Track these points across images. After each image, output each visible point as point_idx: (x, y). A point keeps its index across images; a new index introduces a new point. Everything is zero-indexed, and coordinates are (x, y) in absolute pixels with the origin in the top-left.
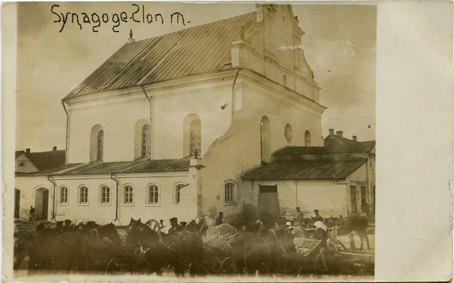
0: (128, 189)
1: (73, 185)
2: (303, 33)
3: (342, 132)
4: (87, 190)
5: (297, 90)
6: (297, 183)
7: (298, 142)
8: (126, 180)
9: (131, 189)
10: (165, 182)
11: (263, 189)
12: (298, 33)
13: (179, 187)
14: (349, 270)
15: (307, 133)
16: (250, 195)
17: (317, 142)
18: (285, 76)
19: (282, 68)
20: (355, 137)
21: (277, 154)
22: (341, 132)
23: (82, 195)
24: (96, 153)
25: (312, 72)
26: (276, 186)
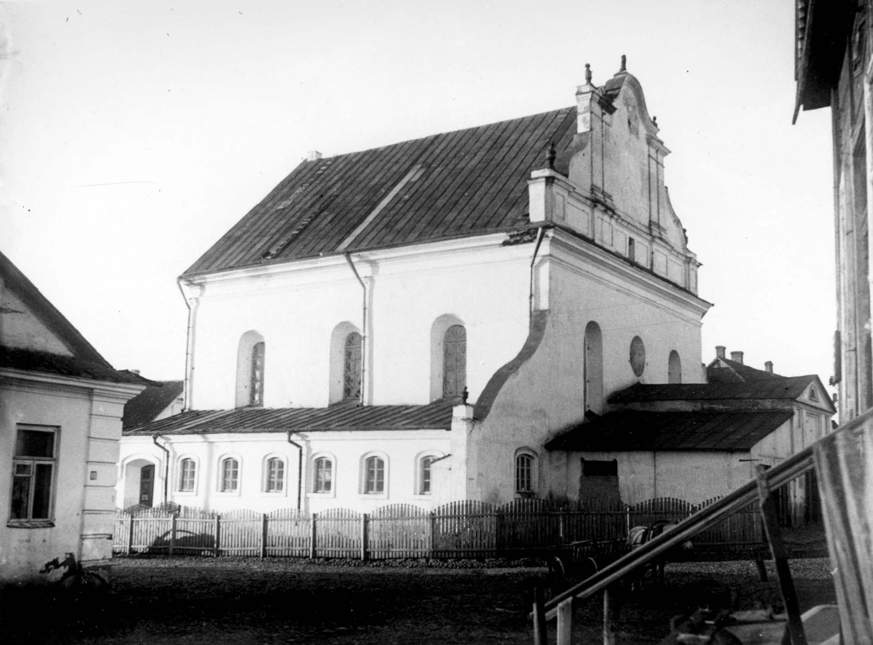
0: (322, 464)
1: (186, 445)
2: (666, 152)
3: (742, 354)
4: (236, 464)
5: (606, 185)
6: (657, 458)
7: (657, 374)
8: (321, 443)
10: (400, 448)
11: (590, 470)
12: (657, 151)
13: (427, 462)
16: (564, 479)
17: (693, 376)
18: (631, 241)
19: (625, 224)
20: (769, 364)
21: (618, 397)
22: (741, 354)
25: (684, 231)
26: (614, 464)
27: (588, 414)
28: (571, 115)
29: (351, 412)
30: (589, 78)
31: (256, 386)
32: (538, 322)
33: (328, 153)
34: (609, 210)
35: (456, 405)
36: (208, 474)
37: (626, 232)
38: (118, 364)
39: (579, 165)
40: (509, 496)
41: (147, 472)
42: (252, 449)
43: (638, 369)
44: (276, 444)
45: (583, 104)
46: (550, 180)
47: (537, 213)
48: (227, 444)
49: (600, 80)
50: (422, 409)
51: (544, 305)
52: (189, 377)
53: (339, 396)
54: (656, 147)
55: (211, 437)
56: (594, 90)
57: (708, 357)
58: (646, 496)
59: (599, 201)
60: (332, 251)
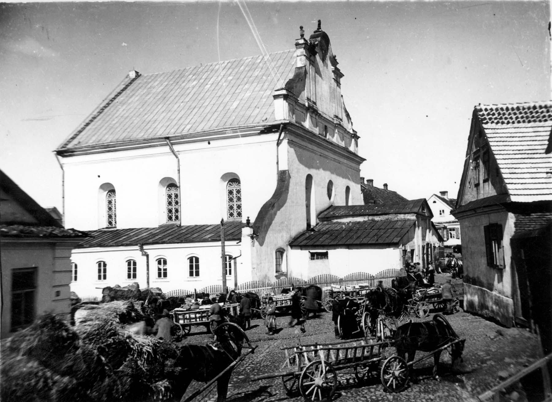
8: (155, 251)
9: (165, 262)
10: (209, 254)
14: (69, 372)
20: (386, 185)
22: (372, 181)
23: (191, 267)
24: (436, 201)
35: (243, 227)
37: (323, 122)
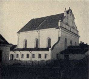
0: (34, 55)
1: (18, 52)
7: (73, 44)
8: (34, 52)
10: (43, 53)
15: (76, 42)
16: (62, 57)
17: (77, 45)
21: (68, 47)
27: (65, 49)
28: (64, 14)
29: (37, 49)
30: (66, 9)
31: (26, 46)
32: (59, 38)
33: (35, 18)
34: (68, 25)
36: (20, 56)
38: (9, 43)
39: (64, 20)
40: (56, 58)
41: (13, 55)
42: (25, 53)
43: (71, 44)
44: (28, 52)
45: (65, 13)
46: (61, 22)
47: (59, 25)
48: (22, 52)
49: (67, 10)
50: (45, 48)
51: (60, 36)
52: (18, 44)
53: (36, 47)
54: (74, 18)
55: (20, 51)
56: (66, 11)
57: (80, 43)
58: (72, 59)
59: (67, 24)
60: (35, 30)
